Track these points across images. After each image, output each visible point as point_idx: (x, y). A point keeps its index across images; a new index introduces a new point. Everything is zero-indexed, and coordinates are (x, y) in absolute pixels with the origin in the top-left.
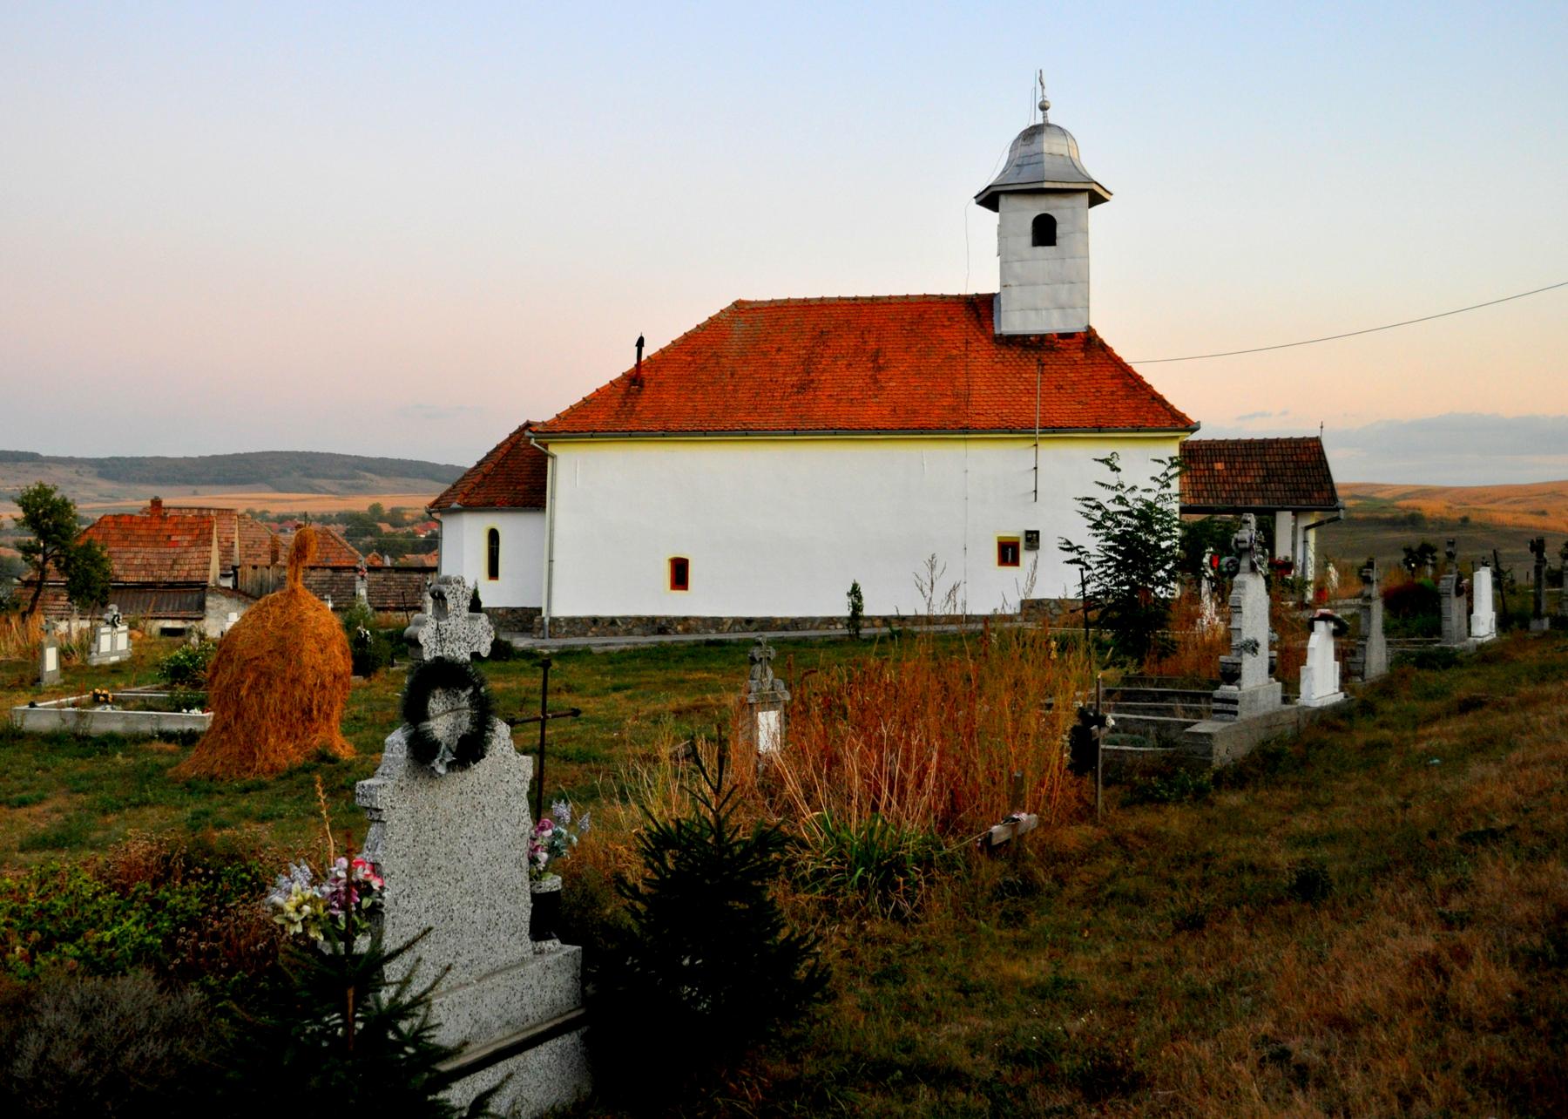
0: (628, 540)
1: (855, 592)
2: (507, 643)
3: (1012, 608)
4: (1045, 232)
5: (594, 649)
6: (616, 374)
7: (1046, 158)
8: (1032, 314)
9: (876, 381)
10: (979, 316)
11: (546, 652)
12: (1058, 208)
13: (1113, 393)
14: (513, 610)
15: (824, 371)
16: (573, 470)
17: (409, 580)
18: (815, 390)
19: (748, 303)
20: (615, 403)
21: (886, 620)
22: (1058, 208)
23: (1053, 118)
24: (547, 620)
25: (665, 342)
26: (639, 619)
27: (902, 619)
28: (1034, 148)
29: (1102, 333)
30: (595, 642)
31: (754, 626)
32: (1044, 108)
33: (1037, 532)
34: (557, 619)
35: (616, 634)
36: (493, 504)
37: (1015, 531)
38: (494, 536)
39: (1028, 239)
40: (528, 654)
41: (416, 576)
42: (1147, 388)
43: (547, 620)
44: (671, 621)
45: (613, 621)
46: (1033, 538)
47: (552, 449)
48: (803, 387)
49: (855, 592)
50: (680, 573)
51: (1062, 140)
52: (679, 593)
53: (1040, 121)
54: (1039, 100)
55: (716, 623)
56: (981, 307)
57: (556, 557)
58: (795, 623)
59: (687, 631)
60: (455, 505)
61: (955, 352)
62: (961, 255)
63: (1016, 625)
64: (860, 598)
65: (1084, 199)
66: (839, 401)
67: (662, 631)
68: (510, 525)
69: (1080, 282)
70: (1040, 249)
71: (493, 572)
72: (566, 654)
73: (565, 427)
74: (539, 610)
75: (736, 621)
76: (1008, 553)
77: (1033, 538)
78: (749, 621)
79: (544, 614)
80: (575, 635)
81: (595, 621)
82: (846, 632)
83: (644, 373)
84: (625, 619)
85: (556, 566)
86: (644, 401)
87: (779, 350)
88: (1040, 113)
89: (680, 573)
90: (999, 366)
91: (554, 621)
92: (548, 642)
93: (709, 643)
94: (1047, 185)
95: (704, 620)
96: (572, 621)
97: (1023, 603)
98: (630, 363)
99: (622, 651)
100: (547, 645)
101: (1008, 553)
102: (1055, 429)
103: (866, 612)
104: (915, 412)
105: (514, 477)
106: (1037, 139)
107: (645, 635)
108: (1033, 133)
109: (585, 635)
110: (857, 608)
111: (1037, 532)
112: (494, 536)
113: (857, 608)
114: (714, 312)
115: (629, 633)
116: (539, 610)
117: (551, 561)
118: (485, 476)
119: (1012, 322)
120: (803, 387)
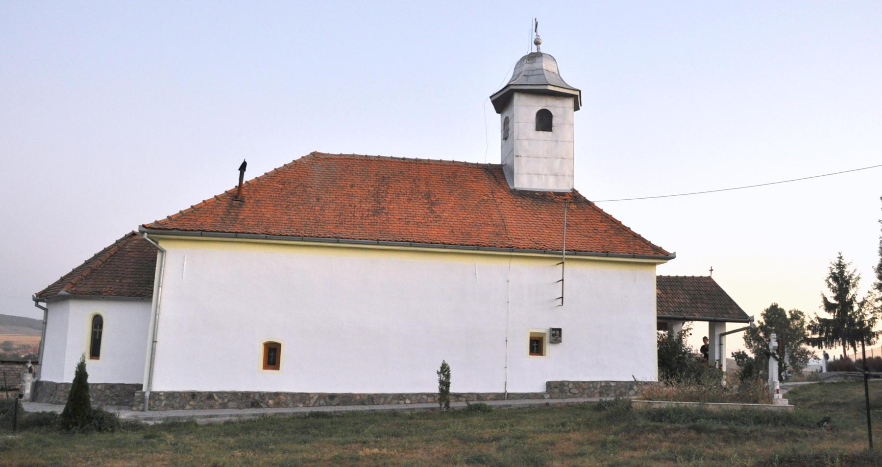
0: (214, 330)
1: (445, 370)
2: (112, 415)
3: (539, 387)
4: (545, 121)
5: (199, 421)
6: (220, 191)
7: (545, 72)
8: (535, 178)
9: (432, 212)
10: (495, 177)
11: (151, 423)
12: (559, 108)
13: (605, 231)
14: (113, 386)
15: (390, 202)
16: (180, 267)
17: (12, 369)
18: (387, 214)
19: (322, 154)
20: (220, 211)
21: (468, 396)
22: (559, 108)
23: (543, 49)
24: (147, 395)
25: (260, 174)
26: (235, 394)
27: (479, 396)
28: (536, 65)
29: (583, 192)
30: (200, 415)
31: (337, 400)
32: (537, 43)
33: (560, 330)
34: (157, 394)
35: (212, 407)
36: (99, 293)
37: (542, 327)
38: (97, 322)
39: (533, 126)
40: (134, 426)
41: (17, 366)
42: (627, 230)
43: (147, 395)
44: (263, 396)
45: (210, 396)
46: (556, 335)
47: (162, 245)
48: (377, 212)
49: (445, 370)
50: (272, 356)
51: (553, 63)
52: (271, 373)
53: (535, 50)
54: (534, 37)
55: (304, 398)
56: (497, 174)
57: (159, 338)
58: (371, 399)
59: (278, 404)
60: (63, 292)
61: (486, 198)
62: (477, 141)
63: (544, 402)
64: (448, 377)
65: (570, 103)
66: (408, 223)
67: (255, 404)
68: (116, 315)
69: (568, 159)
70: (541, 133)
71: (95, 352)
72: (172, 426)
73: (175, 225)
74: (140, 387)
75: (321, 396)
76: (536, 346)
77: (556, 335)
78: (332, 396)
79: (144, 389)
80: (173, 408)
81: (193, 395)
82: (437, 405)
83: (244, 192)
84: (221, 394)
85: (158, 347)
86: (246, 212)
87: (352, 186)
88: (535, 47)
89: (272, 356)
90: (520, 209)
91: (155, 395)
92: (149, 414)
93: (317, 415)
94: (550, 88)
95: (293, 395)
96: (171, 395)
97: (549, 385)
98: (232, 183)
99: (227, 423)
100: (153, 417)
101: (536, 346)
102: (576, 252)
103: (452, 390)
104: (468, 234)
105: (125, 271)
106: (538, 60)
107: (239, 408)
108: (533, 57)
109: (183, 408)
110: (445, 384)
111: (560, 330)
112: (97, 322)
113: (445, 384)
114: (297, 157)
115: (224, 406)
116: (140, 387)
117: (154, 342)
118: (93, 271)
119: (522, 182)
120: (377, 212)
